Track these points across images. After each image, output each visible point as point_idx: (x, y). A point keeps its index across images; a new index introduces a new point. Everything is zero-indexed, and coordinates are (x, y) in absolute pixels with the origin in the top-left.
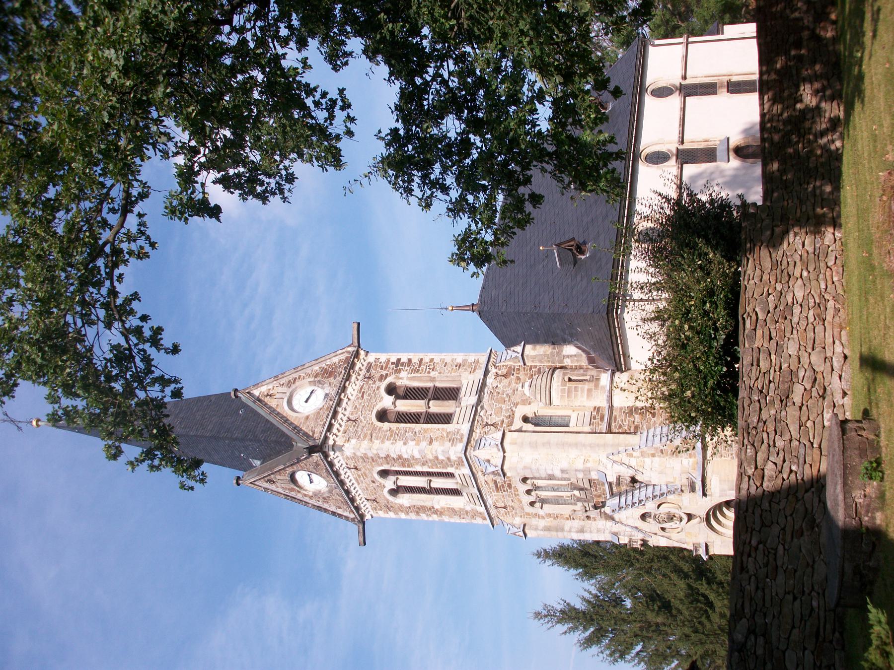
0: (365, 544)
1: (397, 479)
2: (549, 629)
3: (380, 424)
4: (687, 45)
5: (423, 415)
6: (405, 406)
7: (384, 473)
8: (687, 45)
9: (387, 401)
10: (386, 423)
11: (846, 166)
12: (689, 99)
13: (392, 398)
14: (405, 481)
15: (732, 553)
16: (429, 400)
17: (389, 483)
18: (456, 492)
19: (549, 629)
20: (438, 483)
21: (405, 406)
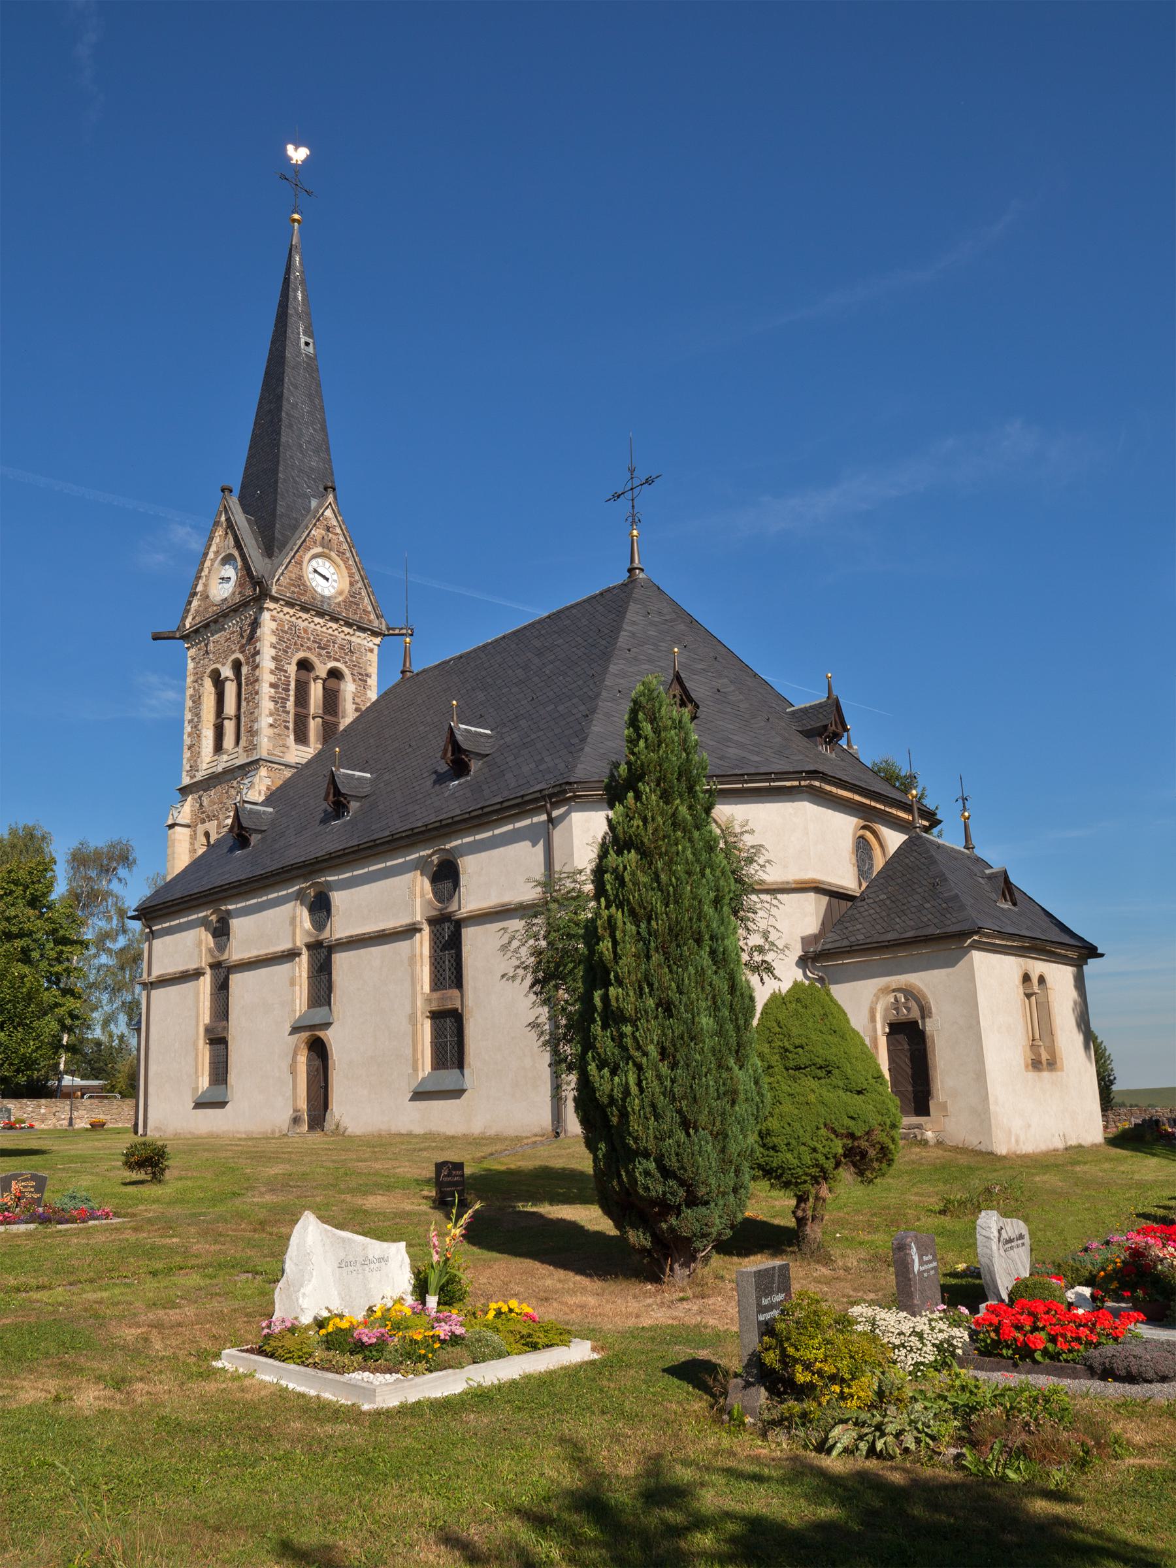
0: (154, 639)
1: (233, 681)
2: (767, 850)
3: (294, 661)
4: (222, 988)
5: (304, 711)
6: (316, 691)
7: (237, 666)
8: (222, 988)
9: (322, 670)
10: (296, 668)
11: (41, 1142)
12: (153, 992)
13: (324, 675)
14: (230, 689)
15: (403, 1244)
16: (322, 718)
17: (227, 672)
18: (218, 747)
19: (767, 850)
20: (229, 726)
21: (316, 691)
